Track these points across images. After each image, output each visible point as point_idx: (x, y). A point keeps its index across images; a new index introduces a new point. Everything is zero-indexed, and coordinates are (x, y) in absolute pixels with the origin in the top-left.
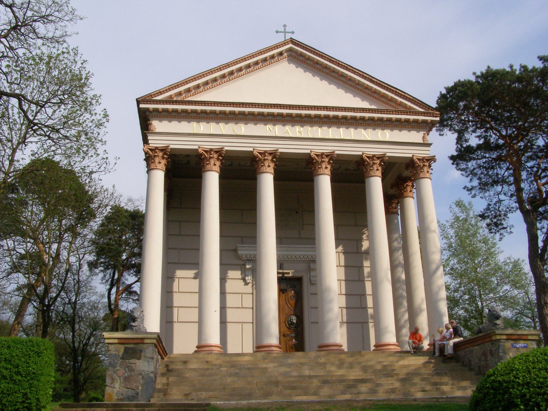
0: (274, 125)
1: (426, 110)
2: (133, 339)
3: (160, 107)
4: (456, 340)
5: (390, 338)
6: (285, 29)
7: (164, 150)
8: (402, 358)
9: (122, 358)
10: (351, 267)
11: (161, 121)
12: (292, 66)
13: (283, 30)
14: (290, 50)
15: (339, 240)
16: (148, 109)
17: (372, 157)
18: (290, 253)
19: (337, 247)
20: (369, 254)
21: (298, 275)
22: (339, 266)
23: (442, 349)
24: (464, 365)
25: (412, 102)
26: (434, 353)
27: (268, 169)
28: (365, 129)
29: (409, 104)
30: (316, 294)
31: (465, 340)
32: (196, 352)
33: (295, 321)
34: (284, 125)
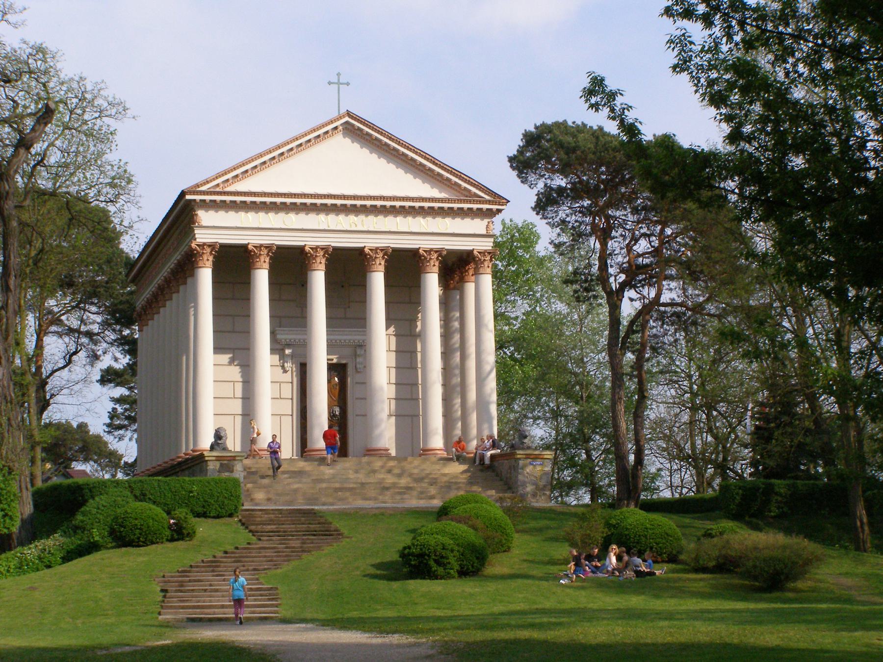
0: (327, 215)
1: (491, 197)
4: (493, 452)
5: (437, 442)
6: (339, 80)
7: (212, 246)
8: (444, 465)
9: (219, 472)
10: (402, 335)
11: (207, 211)
12: (348, 141)
13: (336, 81)
14: (347, 122)
15: (389, 321)
17: (429, 251)
19: (387, 328)
20: (421, 336)
21: (344, 362)
22: (389, 350)
23: (482, 458)
24: (497, 475)
25: (477, 188)
26: (475, 462)
27: (320, 265)
28: (424, 218)
29: (474, 190)
30: (364, 383)
31: (502, 453)
33: (337, 413)
34: (337, 215)
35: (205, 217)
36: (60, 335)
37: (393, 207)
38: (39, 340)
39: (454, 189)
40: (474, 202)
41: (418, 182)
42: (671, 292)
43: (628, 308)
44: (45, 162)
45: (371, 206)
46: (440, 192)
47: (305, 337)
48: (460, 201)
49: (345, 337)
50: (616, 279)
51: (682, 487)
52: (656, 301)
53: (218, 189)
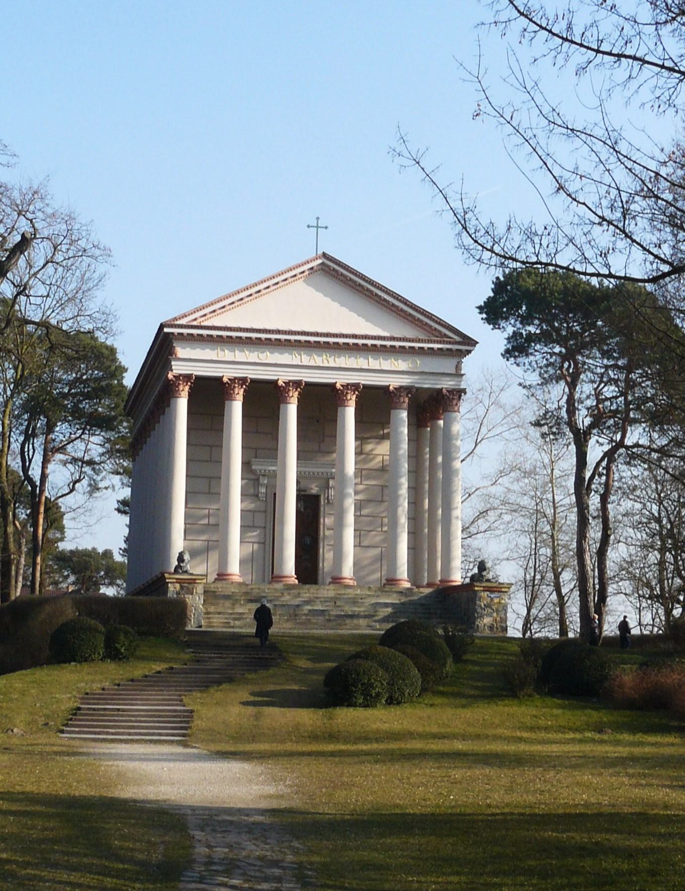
2: (188, 579)
3: (185, 331)
6: (321, 227)
16: (173, 333)
18: (306, 469)
32: (216, 579)
35: (182, 351)
36: (65, 463)
37: (365, 345)
38: (44, 467)
39: (425, 330)
40: (447, 343)
41: (361, 320)
42: (636, 435)
43: (596, 450)
44: (27, 292)
45: (372, 345)
46: (384, 330)
47: (300, 469)
48: (429, 341)
49: (315, 470)
50: (583, 419)
51: (653, 626)
52: (621, 444)
53: (195, 323)
